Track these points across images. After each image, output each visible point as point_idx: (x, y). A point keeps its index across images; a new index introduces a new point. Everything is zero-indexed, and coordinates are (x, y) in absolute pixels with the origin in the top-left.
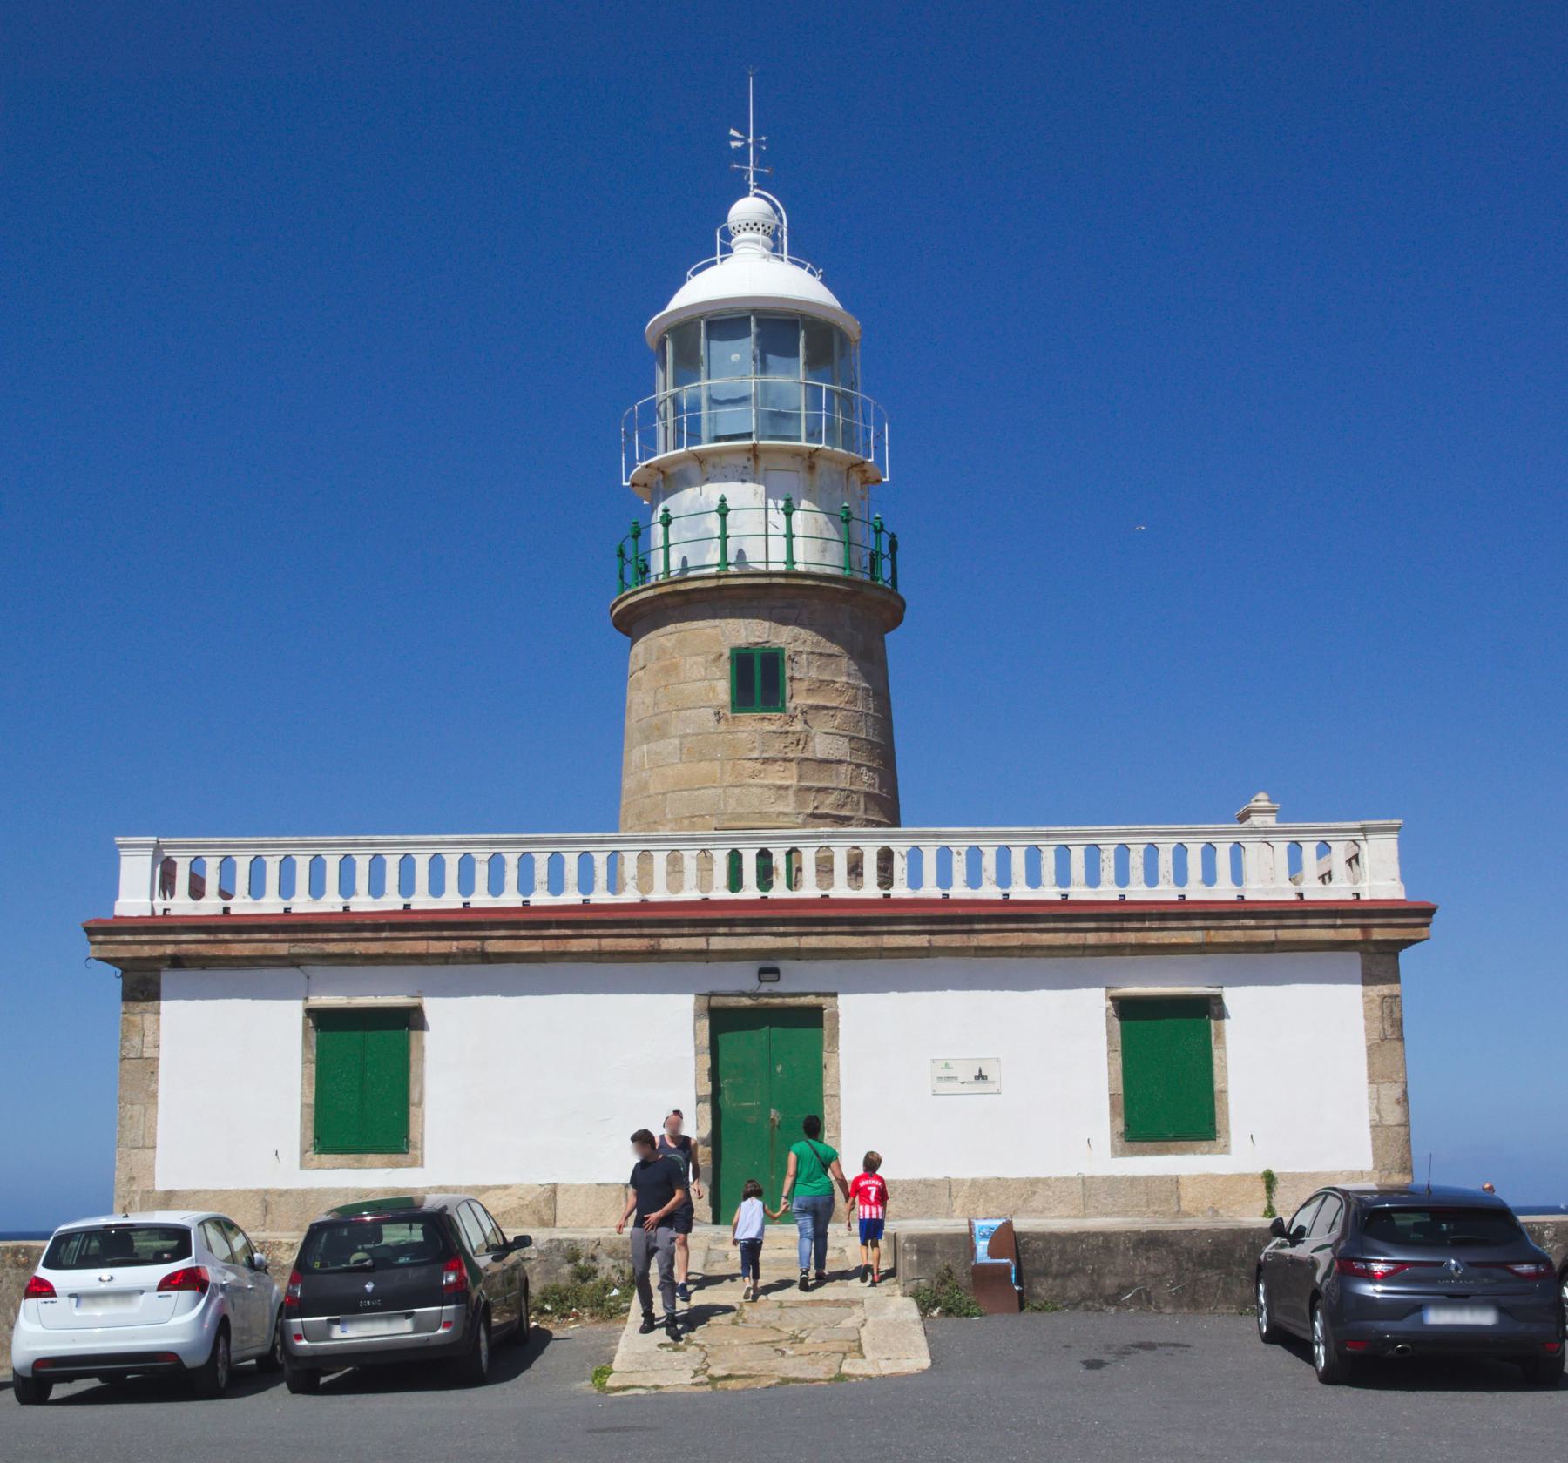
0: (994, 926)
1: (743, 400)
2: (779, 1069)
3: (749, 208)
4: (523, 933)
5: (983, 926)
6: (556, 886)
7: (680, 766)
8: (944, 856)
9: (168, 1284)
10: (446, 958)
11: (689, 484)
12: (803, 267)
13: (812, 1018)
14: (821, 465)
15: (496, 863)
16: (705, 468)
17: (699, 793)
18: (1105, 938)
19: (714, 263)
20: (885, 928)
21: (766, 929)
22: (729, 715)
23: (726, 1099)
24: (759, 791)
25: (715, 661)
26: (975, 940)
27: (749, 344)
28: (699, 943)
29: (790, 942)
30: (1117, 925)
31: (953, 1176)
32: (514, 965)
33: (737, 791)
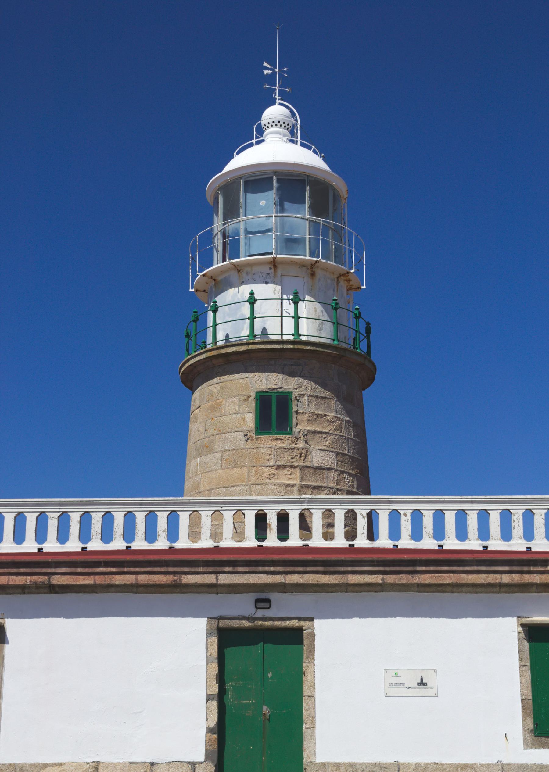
0: (432, 568)
1: (268, 231)
2: (270, 675)
3: (275, 112)
4: (79, 570)
5: (424, 568)
6: (107, 536)
7: (220, 471)
8: (395, 517)
10: (23, 589)
11: (231, 286)
12: (309, 148)
13: (295, 638)
14: (319, 273)
15: (64, 520)
16: (242, 274)
17: (230, 484)
18: (516, 578)
19: (251, 145)
20: (349, 569)
21: (261, 569)
22: (254, 436)
23: (230, 697)
24: (273, 487)
25: (245, 400)
26: (418, 579)
27: (272, 195)
28: (210, 579)
29: (279, 579)
30: (526, 569)
31: (401, 761)
32: (74, 595)
33: (258, 487)
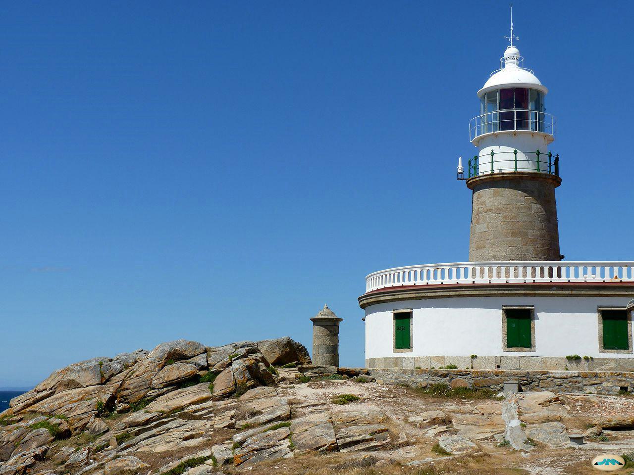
3: (511, 51)
9: (260, 413)
12: (529, 71)
